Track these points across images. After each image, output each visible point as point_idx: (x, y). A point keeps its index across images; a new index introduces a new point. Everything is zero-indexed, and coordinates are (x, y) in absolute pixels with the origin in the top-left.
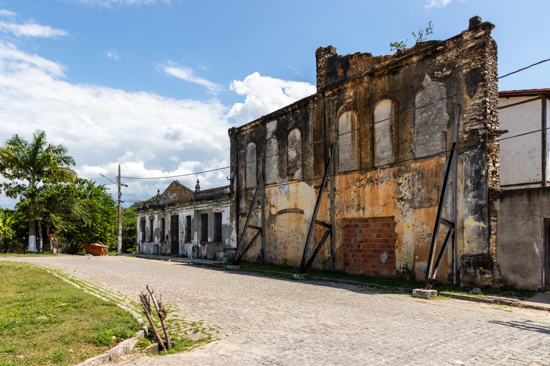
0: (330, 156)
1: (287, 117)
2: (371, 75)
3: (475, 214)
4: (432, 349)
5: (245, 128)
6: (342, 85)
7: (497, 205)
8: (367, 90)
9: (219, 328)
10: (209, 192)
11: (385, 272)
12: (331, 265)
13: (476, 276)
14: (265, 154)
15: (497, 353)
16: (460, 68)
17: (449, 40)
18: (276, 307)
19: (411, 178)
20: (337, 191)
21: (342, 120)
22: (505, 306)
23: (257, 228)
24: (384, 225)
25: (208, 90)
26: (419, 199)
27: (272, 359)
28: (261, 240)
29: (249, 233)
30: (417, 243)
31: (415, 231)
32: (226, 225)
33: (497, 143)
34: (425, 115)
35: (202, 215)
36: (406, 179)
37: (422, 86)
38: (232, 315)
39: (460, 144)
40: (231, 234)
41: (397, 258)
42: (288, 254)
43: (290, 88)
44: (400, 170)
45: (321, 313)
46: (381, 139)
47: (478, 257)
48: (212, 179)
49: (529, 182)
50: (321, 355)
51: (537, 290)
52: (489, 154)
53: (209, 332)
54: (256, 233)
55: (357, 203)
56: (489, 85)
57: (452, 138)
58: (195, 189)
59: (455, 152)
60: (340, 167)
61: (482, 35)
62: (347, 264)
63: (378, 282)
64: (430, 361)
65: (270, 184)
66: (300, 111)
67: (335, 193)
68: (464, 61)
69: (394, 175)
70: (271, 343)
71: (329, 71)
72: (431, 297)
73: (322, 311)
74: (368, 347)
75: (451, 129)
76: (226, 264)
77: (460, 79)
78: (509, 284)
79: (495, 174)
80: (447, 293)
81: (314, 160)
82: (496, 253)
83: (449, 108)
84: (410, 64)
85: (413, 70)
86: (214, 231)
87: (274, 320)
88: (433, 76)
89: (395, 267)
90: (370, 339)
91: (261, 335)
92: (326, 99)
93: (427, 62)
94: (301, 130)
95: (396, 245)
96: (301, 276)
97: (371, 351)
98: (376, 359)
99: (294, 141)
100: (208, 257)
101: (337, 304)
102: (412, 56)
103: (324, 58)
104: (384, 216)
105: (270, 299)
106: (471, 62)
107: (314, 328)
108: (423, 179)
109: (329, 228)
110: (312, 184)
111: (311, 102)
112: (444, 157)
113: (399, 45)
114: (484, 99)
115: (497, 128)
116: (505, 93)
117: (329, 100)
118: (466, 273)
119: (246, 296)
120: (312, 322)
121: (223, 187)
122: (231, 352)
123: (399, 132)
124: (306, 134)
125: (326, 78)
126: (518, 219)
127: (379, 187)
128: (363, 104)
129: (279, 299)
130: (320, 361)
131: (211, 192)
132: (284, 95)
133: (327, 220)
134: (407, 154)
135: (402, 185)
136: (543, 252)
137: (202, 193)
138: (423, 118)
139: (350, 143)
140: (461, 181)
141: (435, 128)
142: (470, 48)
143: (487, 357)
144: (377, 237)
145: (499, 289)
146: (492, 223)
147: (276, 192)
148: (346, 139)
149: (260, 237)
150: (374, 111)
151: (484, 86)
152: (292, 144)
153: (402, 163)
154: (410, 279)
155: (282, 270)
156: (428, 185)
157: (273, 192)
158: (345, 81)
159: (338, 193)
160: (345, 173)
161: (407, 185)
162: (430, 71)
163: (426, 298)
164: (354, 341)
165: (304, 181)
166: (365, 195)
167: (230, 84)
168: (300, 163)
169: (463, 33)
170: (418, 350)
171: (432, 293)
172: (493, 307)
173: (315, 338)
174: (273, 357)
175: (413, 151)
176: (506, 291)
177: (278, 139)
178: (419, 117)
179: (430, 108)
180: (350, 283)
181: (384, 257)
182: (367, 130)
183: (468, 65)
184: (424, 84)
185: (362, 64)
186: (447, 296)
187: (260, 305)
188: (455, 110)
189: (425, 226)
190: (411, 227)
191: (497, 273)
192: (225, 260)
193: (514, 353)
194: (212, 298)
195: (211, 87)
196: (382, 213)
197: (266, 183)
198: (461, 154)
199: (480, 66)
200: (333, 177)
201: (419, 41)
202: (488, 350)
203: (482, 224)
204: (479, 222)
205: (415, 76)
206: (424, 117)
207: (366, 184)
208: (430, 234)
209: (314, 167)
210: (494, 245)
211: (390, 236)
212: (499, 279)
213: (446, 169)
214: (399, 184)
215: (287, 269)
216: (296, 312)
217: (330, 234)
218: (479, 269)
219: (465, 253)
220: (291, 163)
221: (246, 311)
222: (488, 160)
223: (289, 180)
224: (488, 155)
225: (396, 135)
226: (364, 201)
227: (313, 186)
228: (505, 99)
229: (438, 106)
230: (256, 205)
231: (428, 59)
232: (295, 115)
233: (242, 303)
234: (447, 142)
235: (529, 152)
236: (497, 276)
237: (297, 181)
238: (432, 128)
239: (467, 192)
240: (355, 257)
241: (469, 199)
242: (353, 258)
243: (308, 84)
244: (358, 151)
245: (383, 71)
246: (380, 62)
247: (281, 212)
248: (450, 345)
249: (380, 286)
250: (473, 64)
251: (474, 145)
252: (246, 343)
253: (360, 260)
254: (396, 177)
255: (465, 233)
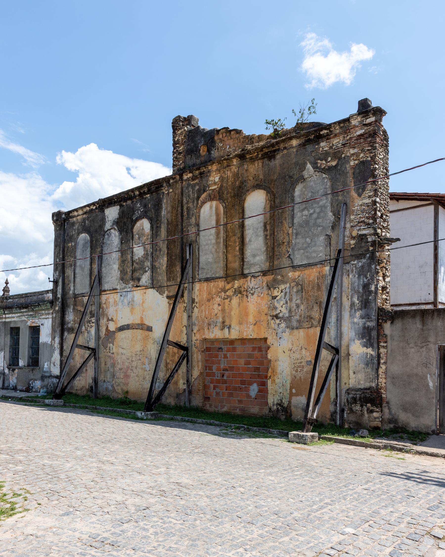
0: (188, 257)
1: (132, 202)
2: (242, 157)
3: (363, 338)
4: (316, 514)
5: (76, 213)
6: (205, 166)
7: (387, 328)
8: (236, 175)
9: (28, 492)
10: (23, 297)
11: (255, 410)
12: (187, 400)
13: (362, 415)
14: (102, 250)
15: (394, 516)
16: (347, 160)
17: (335, 123)
18: (112, 459)
19: (288, 290)
20: (197, 303)
21: (204, 212)
22: (396, 452)
23: (89, 348)
24: (254, 349)
25: (25, 161)
26: (298, 317)
27: (104, 538)
28: (93, 365)
29: (77, 355)
30: (294, 372)
31: (292, 358)
32: (45, 344)
33: (387, 253)
34: (306, 212)
35: (12, 328)
36: (282, 292)
37: (303, 176)
38: (48, 472)
39: (346, 251)
40: (52, 356)
41: (270, 392)
42: (129, 385)
43: (136, 168)
44: (275, 280)
45: (173, 467)
46: (253, 240)
47: (365, 391)
48: (29, 281)
49: (420, 302)
50: (173, 528)
51: (430, 432)
52: (379, 265)
53: (12, 500)
54: (87, 356)
55: (221, 320)
56: (379, 183)
57: (337, 243)
58: (2, 293)
59: (340, 261)
60: (200, 272)
61: (372, 122)
62: (207, 399)
63: (246, 422)
64: (315, 531)
65: (108, 290)
66: (150, 196)
67: (194, 305)
68: (352, 151)
69: (268, 286)
70: (103, 514)
71: (189, 147)
72: (311, 442)
73: (174, 463)
74: (236, 514)
75: (336, 232)
76: (44, 397)
77: (347, 172)
78: (400, 425)
79: (385, 290)
80: (330, 436)
81: (167, 261)
82: (385, 387)
83: (334, 207)
84: (289, 149)
85: (293, 156)
86: (29, 351)
87: (108, 479)
88: (315, 166)
89: (267, 403)
90: (238, 502)
91: (89, 502)
92: (184, 183)
93: (310, 148)
94: (151, 220)
95: (269, 374)
96: (148, 414)
97: (240, 520)
98: (247, 531)
99: (141, 235)
100: (19, 387)
101: (195, 453)
102: (291, 139)
103: (182, 130)
104: (255, 337)
105: (103, 448)
106: (360, 153)
107: (164, 489)
108: (302, 292)
109: (184, 351)
110: (164, 293)
111: (165, 185)
112: (327, 266)
113: (276, 123)
114: (374, 199)
115: (388, 235)
116: (395, 195)
117: (189, 185)
118: (351, 411)
119: (70, 444)
120: (161, 480)
121: (43, 291)
122: (44, 530)
123: (274, 232)
124: (157, 227)
125: (185, 156)
126: (411, 345)
127: (249, 300)
128: (230, 193)
129: (117, 447)
130: (172, 538)
131: (26, 297)
132: (129, 176)
133: (182, 340)
134: (284, 259)
135: (278, 298)
136: (437, 387)
137: (12, 299)
138: (304, 217)
139: (214, 241)
140: (347, 296)
141: (317, 229)
142: (359, 136)
143: (382, 522)
144: (245, 364)
145: (389, 431)
146: (382, 350)
147: (115, 301)
148: (209, 237)
149: (92, 360)
150: (244, 203)
151: (374, 182)
152: (139, 238)
153: (278, 271)
154: (285, 419)
155: (122, 406)
156: (308, 300)
157: (111, 300)
158: (209, 161)
159: (197, 305)
160: (207, 280)
161: (283, 299)
162: (312, 159)
163: (305, 444)
164: (217, 506)
165: (153, 288)
166: (231, 310)
167: (57, 155)
168: (149, 264)
169: (352, 116)
170: (299, 516)
171: (313, 437)
172: (384, 454)
173: (165, 503)
174: (105, 535)
175: (292, 257)
176: (397, 434)
177: (121, 231)
178: (299, 214)
179: (312, 205)
180: (211, 424)
181: (254, 389)
182: (235, 226)
183: (356, 156)
184: (306, 174)
185: (231, 142)
186: (330, 440)
187: (90, 456)
188: (341, 209)
189: (304, 350)
190: (287, 353)
191: (386, 410)
192: (42, 392)
193: (413, 515)
194: (20, 447)
195: (29, 157)
196: (252, 334)
197: (103, 289)
198: (347, 263)
199: (369, 159)
200: (191, 284)
201: (299, 122)
202: (383, 512)
203: (370, 351)
204: (367, 348)
205: (295, 163)
206: (305, 216)
207: (233, 295)
208: (310, 361)
209: (167, 270)
210: (384, 376)
211: (262, 363)
212: (388, 419)
213: (329, 282)
214: (274, 298)
215: (128, 404)
216: (140, 465)
217: (186, 359)
218: (366, 406)
219: (351, 386)
220: (137, 263)
221: (68, 465)
222: (378, 272)
223: (133, 286)
224: (378, 267)
225: (271, 235)
226: (230, 317)
227: (165, 295)
228: (395, 202)
229: (321, 203)
230: (87, 318)
231: (310, 144)
232: (144, 201)
233: (63, 454)
234: (332, 248)
235: (420, 267)
236: (387, 416)
237: (144, 288)
238: (314, 230)
239: (353, 310)
240: (218, 390)
241: (356, 320)
242: (215, 391)
243: (161, 165)
244: (224, 252)
245: (256, 154)
246: (253, 143)
247: (122, 329)
248: (338, 507)
249: (248, 428)
250: (362, 155)
251: (362, 254)
252: (67, 514)
253: (223, 393)
254: (270, 289)
255: (350, 361)
